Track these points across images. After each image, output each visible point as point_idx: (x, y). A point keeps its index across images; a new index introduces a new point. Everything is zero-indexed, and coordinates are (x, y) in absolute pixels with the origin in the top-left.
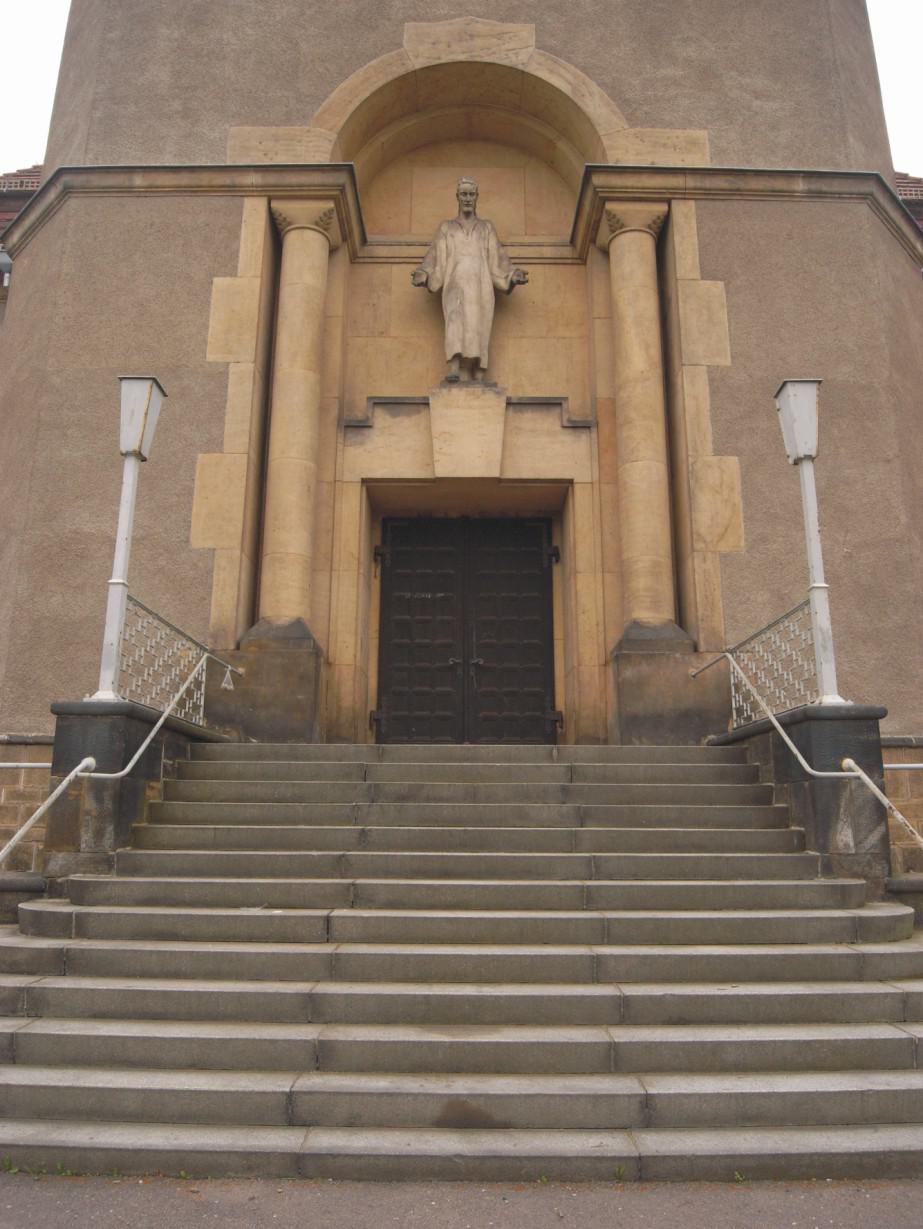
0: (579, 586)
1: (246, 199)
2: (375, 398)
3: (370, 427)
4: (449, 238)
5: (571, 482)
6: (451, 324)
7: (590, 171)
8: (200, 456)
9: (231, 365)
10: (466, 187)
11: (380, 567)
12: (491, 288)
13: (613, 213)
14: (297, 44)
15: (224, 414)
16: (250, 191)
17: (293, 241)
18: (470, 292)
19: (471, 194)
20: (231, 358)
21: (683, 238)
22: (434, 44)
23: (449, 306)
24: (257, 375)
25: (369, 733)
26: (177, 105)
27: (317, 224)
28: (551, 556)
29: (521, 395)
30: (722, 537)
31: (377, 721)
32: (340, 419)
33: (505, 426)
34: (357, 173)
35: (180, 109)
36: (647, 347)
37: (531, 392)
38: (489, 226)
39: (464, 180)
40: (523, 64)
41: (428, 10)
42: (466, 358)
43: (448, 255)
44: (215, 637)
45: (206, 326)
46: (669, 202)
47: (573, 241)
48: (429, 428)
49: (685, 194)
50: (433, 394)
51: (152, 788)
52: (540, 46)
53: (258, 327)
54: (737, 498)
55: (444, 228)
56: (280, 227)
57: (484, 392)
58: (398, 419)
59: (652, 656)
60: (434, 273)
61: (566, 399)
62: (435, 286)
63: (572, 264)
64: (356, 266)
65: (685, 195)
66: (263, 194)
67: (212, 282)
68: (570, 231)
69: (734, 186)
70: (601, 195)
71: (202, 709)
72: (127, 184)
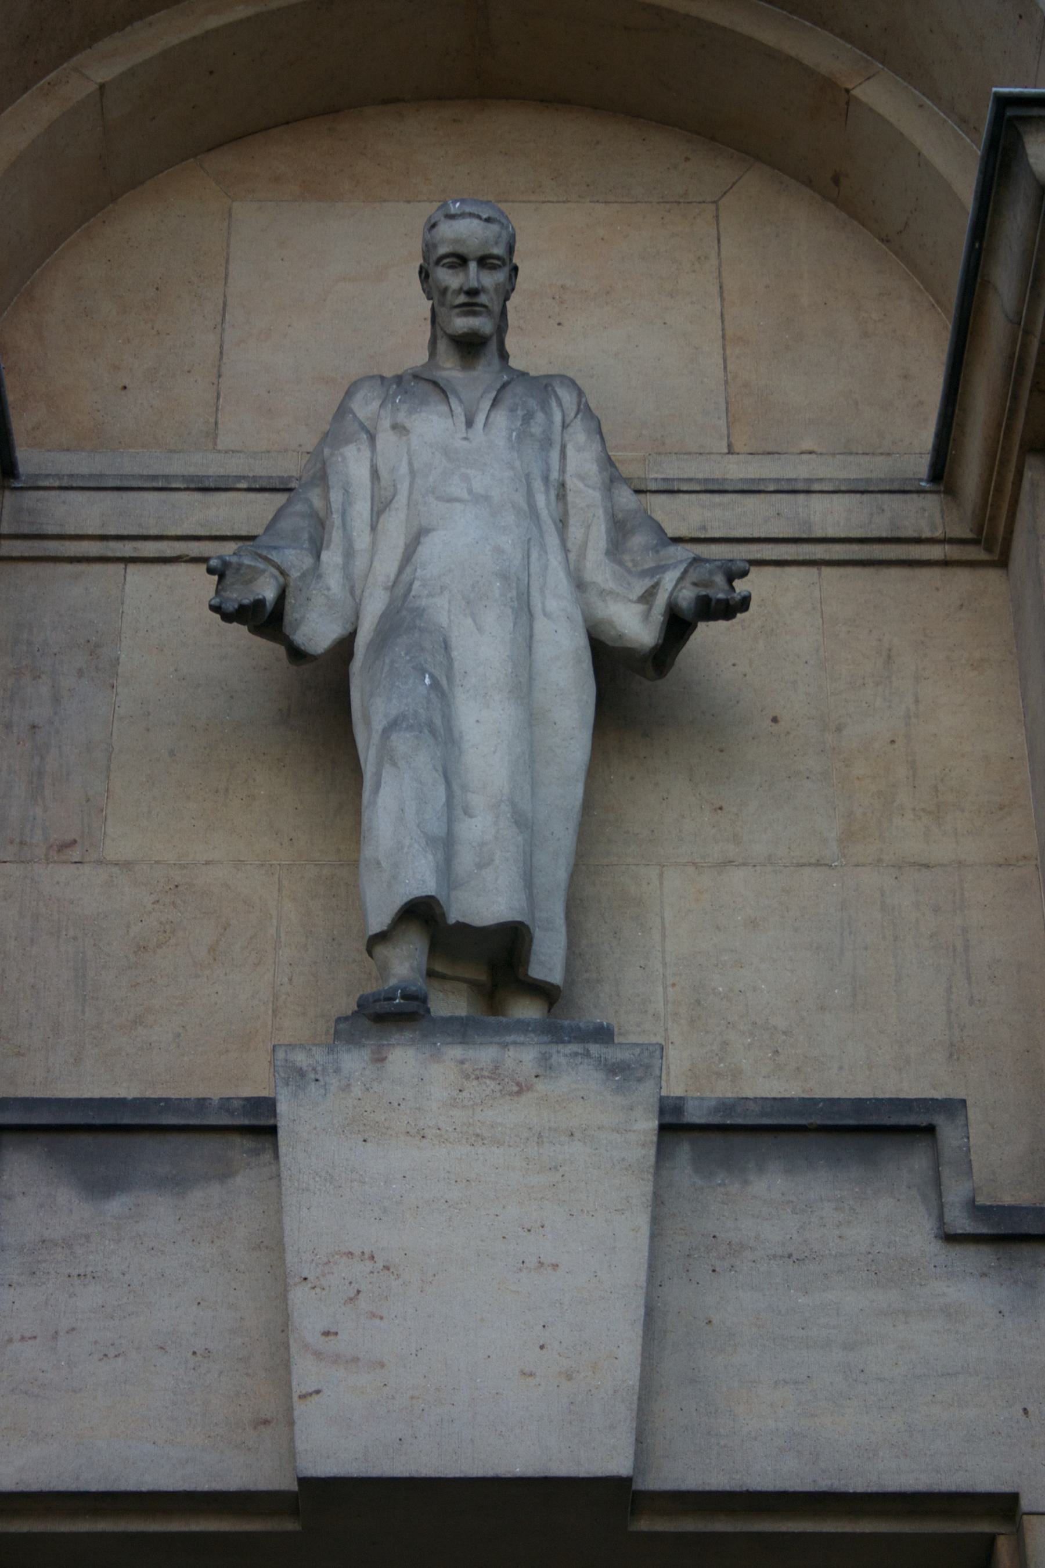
4: (386, 439)
6: (388, 775)
12: (583, 642)
19: (485, 262)
29: (724, 1090)
33: (656, 1220)
38: (567, 397)
39: (456, 207)
42: (463, 928)
43: (380, 508)
50: (298, 1076)
57: (546, 1067)
58: (115, 1206)
60: (315, 571)
61: (954, 1107)
63: (945, 563)
68: (927, 437)
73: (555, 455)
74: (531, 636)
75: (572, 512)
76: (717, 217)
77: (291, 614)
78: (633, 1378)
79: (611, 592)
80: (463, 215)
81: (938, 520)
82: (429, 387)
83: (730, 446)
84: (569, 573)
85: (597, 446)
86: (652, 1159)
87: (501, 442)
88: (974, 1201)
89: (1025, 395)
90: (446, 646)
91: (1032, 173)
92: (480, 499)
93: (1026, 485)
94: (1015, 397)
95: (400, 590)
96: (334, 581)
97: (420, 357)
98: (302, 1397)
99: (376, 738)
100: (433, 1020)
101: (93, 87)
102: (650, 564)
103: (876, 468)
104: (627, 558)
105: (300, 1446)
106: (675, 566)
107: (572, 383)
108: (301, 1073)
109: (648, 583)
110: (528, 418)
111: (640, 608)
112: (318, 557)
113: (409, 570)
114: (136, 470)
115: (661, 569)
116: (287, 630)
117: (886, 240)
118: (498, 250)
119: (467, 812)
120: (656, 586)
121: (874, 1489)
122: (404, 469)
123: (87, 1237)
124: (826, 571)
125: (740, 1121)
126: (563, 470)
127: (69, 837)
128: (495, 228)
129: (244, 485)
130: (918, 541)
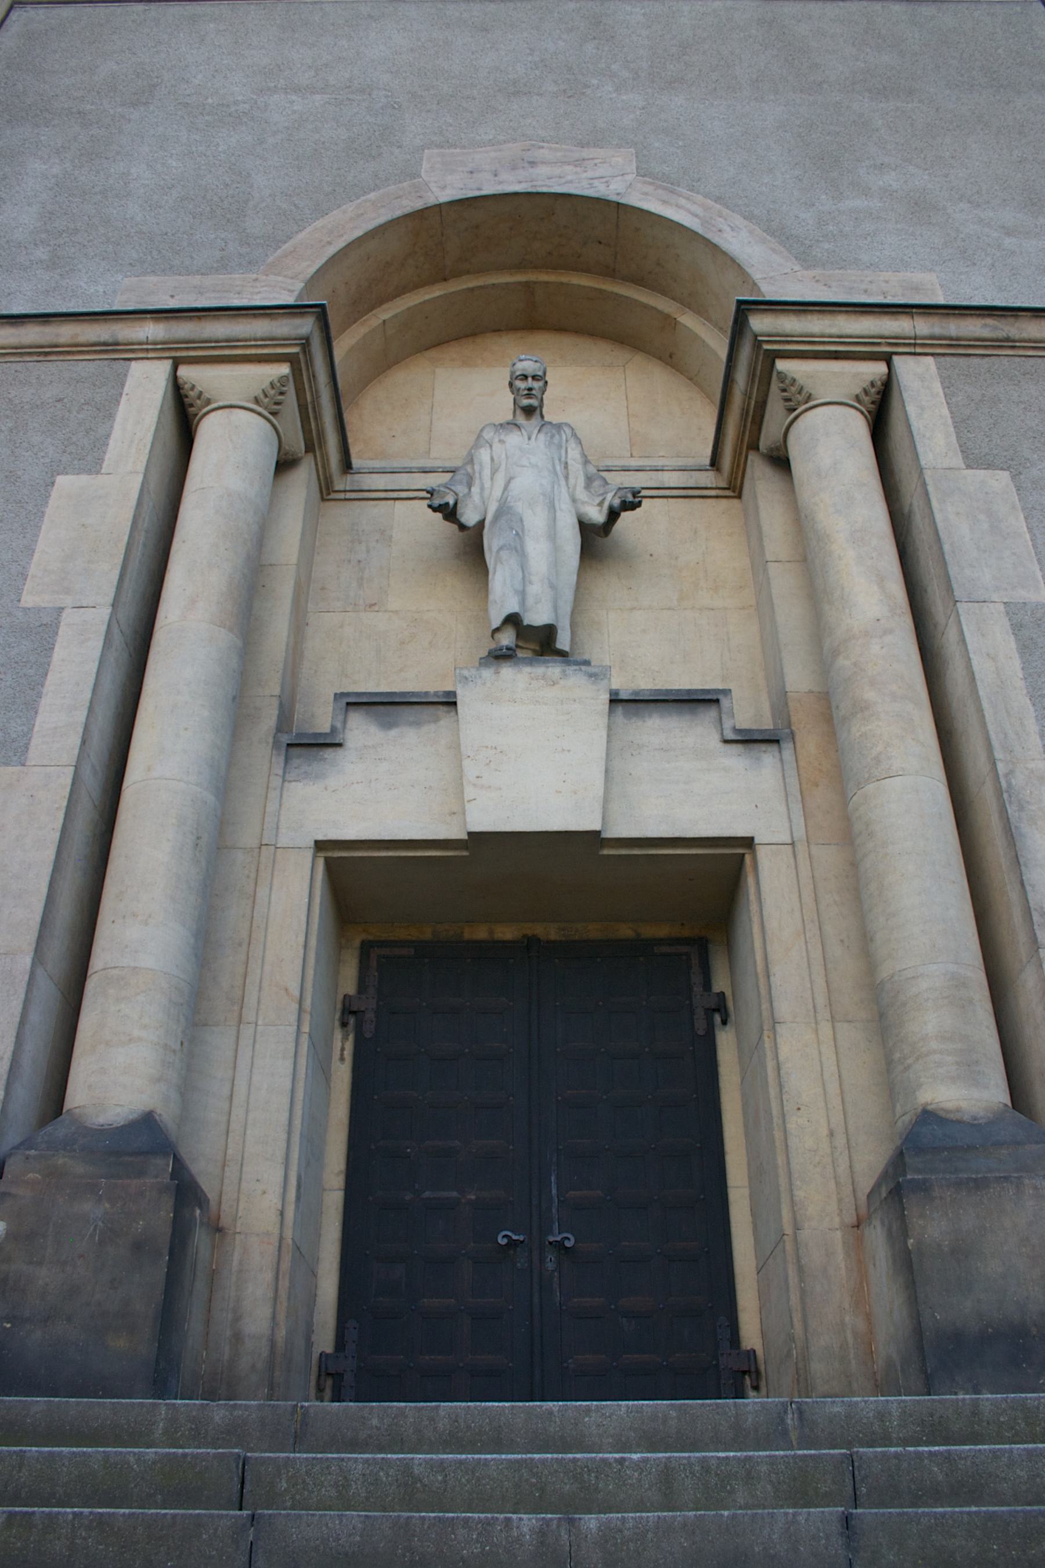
0: (785, 1051)
1: (133, 363)
2: (348, 694)
3: (340, 745)
4: (497, 446)
5: (748, 842)
6: (499, 568)
7: (744, 309)
10: (527, 366)
11: (351, 1037)
12: (576, 521)
13: (790, 375)
14: (249, 175)
16: (142, 350)
18: (535, 521)
19: (534, 378)
20: (68, 601)
21: (922, 408)
23: (491, 543)
24: (118, 639)
26: (41, 253)
27: (257, 401)
28: (710, 1012)
35: (44, 257)
36: (881, 580)
37: (645, 683)
38: (568, 431)
39: (523, 357)
40: (618, 194)
41: (463, 136)
42: (529, 626)
43: (494, 472)
45: (30, 550)
46: (887, 359)
47: (715, 462)
48: (456, 747)
49: (915, 345)
52: (642, 173)
55: (488, 435)
56: (192, 410)
58: (394, 732)
61: (727, 692)
62: (469, 516)
63: (717, 497)
64: (327, 504)
65: (915, 347)
66: (167, 354)
67: (53, 483)
68: (709, 451)
69: (1000, 334)
70: (766, 347)
73: (563, 452)
74: (555, 518)
75: (570, 473)
76: (624, 371)
77: (460, 510)
78: (601, 793)
79: (586, 502)
80: (526, 360)
81: (713, 479)
82: (513, 426)
83: (631, 454)
84: (569, 495)
85: (580, 448)
86: (607, 710)
88: (734, 727)
89: (749, 424)
90: (521, 520)
91: (752, 330)
93: (749, 462)
94: (745, 426)
95: (503, 501)
96: (476, 497)
97: (510, 417)
98: (469, 801)
99: (494, 554)
100: (519, 659)
101: (381, 321)
102: (601, 492)
103: (690, 462)
104: (592, 490)
105: (468, 819)
106: (611, 491)
107: (569, 426)
108: (466, 678)
109: (601, 498)
110: (552, 436)
111: (598, 508)
112: (470, 490)
113: (506, 492)
114: (399, 466)
115: (606, 493)
116: (458, 517)
117: (691, 379)
118: (540, 373)
119: (531, 583)
120: (604, 499)
121: (697, 836)
122: (504, 456)
123: (382, 745)
124: (670, 500)
125: (641, 698)
126: (566, 457)
127: (374, 602)
128: (538, 365)
129: (441, 470)
130: (706, 488)
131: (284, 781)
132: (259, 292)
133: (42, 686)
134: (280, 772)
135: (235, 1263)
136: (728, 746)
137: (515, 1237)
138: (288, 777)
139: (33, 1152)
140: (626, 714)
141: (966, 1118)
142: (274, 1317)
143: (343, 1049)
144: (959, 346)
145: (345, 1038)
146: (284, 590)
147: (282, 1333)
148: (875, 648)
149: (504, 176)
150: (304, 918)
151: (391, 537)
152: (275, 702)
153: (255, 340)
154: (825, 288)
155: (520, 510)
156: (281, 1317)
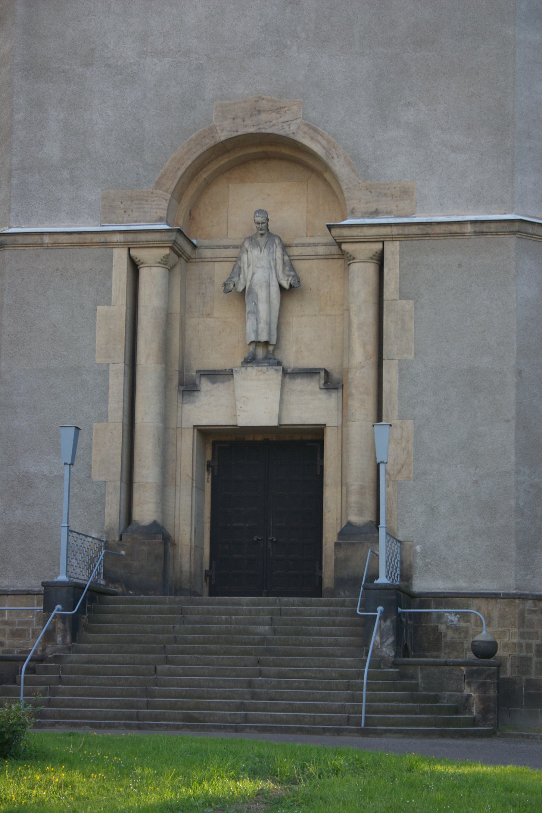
1: (114, 249)
3: (199, 391)
4: (249, 252)
5: (325, 425)
8: (95, 424)
9: (111, 365)
11: (210, 474)
15: (108, 397)
17: (144, 273)
18: (262, 294)
22: (234, 119)
25: (204, 584)
26: (66, 174)
30: (399, 472)
31: (211, 577)
32: (181, 384)
34: (183, 231)
40: (293, 133)
43: (249, 266)
44: (107, 533)
45: (94, 339)
46: (383, 242)
51: (84, 618)
53: (125, 340)
54: (411, 447)
58: (216, 385)
59: (353, 544)
65: (392, 238)
66: (125, 246)
69: (425, 232)
71: (102, 575)
72: (40, 242)
73: (274, 254)
87: (266, 255)
90: (257, 295)
92: (262, 267)
96: (242, 280)
101: (203, 179)
111: (287, 282)
124: (320, 260)
126: (276, 256)
131: (182, 404)
132: (154, 201)
133: (108, 394)
134: (181, 401)
135: (179, 553)
136: (322, 390)
137: (259, 538)
138: (184, 402)
139: (128, 534)
140: (290, 378)
141: (357, 525)
142: (190, 566)
143: (208, 478)
144: (409, 237)
145: (208, 475)
146: (176, 325)
147: (193, 570)
148: (358, 374)
149: (248, 122)
150: (191, 452)
151: (214, 281)
152: (177, 373)
153: (156, 241)
154: (369, 193)
155: (256, 290)
156: (192, 565)
